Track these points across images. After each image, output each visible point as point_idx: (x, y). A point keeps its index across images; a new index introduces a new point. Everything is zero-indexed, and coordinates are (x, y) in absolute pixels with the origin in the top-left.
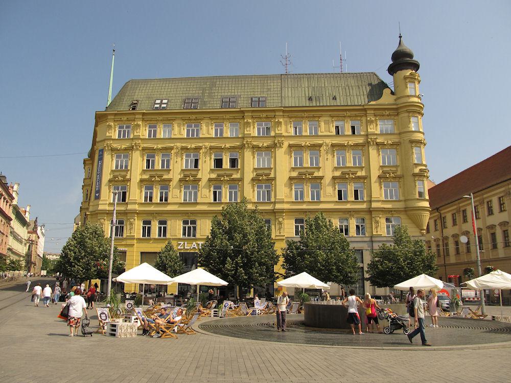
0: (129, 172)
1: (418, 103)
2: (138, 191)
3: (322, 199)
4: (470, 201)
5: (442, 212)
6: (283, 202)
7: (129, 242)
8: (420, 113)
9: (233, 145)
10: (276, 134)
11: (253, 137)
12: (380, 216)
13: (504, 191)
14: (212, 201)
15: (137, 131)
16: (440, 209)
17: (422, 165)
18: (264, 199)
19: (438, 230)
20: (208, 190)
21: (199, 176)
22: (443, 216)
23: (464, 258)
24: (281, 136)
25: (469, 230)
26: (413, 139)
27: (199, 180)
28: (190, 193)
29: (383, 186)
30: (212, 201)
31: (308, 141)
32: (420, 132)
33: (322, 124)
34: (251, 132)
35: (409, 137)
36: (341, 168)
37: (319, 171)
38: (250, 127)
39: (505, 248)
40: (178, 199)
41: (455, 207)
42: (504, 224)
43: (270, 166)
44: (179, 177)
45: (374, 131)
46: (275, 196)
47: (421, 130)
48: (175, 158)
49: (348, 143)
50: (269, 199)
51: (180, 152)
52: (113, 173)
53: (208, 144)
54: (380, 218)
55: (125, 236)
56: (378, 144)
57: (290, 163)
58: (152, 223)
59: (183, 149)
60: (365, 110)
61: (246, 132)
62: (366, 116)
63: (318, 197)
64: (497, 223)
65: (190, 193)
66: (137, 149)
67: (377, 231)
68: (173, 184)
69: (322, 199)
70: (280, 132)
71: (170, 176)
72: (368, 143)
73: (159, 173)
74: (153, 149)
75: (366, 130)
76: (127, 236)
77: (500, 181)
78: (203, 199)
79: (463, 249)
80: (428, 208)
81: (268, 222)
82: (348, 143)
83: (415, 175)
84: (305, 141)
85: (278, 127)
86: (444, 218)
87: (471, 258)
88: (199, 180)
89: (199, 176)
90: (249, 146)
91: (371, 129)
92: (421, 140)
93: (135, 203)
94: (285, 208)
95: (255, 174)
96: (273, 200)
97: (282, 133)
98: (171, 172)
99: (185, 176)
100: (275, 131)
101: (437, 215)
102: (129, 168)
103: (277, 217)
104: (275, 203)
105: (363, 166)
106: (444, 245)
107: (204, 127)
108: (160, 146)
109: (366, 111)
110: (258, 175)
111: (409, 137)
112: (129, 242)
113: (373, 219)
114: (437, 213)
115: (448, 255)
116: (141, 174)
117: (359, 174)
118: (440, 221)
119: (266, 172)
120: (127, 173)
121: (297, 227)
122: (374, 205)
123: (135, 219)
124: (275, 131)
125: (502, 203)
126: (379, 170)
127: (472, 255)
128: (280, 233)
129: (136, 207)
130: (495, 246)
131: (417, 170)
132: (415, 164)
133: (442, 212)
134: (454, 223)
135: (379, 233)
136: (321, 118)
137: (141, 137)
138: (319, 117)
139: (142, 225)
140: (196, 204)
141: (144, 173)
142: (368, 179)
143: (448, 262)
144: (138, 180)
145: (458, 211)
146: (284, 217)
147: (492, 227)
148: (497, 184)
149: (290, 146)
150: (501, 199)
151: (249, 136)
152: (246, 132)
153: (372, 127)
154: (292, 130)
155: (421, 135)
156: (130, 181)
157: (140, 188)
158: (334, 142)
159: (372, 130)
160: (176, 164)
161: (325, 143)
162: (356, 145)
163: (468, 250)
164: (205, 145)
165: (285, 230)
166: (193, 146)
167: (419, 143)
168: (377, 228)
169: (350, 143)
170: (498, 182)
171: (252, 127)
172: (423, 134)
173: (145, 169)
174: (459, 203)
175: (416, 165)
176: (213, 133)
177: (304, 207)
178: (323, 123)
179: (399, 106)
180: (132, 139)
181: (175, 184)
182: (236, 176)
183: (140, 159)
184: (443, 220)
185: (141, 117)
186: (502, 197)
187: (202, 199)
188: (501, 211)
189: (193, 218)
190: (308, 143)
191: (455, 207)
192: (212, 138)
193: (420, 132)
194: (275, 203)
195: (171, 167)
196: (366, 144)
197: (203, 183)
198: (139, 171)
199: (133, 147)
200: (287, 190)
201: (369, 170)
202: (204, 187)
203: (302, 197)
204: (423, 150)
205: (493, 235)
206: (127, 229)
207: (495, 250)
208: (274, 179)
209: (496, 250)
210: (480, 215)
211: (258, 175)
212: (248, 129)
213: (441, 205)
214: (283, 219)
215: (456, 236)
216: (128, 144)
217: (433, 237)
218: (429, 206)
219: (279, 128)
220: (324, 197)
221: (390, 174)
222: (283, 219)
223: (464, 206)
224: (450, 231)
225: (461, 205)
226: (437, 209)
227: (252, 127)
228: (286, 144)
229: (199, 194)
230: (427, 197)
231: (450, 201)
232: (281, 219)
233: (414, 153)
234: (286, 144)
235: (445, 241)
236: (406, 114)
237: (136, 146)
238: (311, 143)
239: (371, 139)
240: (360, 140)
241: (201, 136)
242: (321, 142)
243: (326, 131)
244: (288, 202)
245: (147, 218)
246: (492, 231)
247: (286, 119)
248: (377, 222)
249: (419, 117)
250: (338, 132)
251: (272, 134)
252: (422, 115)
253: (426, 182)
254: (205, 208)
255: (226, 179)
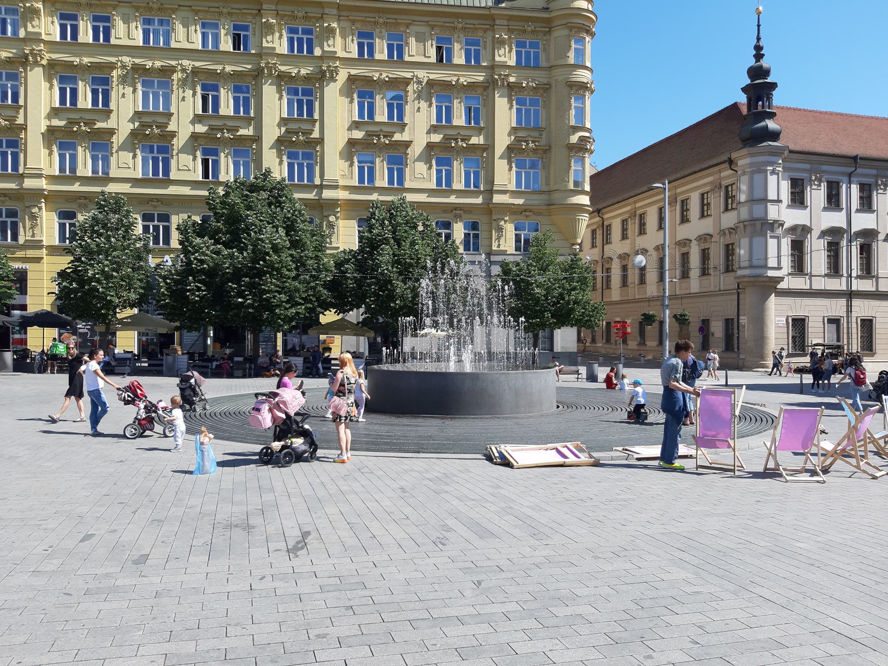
0: (22, 111)
1: (588, 11)
2: (44, 152)
3: (173, 175)
4: (662, 196)
5: (605, 216)
6: (336, 187)
7: (31, 253)
8: (589, 32)
9: (395, 76)
10: (323, 51)
11: (279, 55)
12: (507, 218)
13: (711, 182)
14: (200, 179)
15: (34, 23)
16: (604, 211)
17: (583, 129)
18: (301, 178)
19: (596, 247)
20: (191, 157)
21: (171, 127)
22: (606, 223)
23: (634, 292)
24: (332, 56)
25: (646, 247)
26: (574, 80)
27: (173, 134)
28: (301, 166)
29: (514, 165)
30: (200, 179)
31: (384, 71)
32: (586, 68)
33: (412, 41)
34: (276, 45)
35: (567, 76)
36: (210, 117)
37: (403, 130)
38: (273, 34)
39: (681, 281)
40: (132, 171)
41: (629, 208)
42: (705, 238)
43: (169, 109)
44: (131, 126)
45: (506, 59)
46: (25, 164)
47: (588, 64)
48: (181, 91)
49: (458, 80)
50: (311, 177)
51: (130, 76)
52: (140, 118)
53: (422, 74)
54: (506, 222)
55: (21, 240)
56: (511, 86)
57: (351, 112)
58: (455, 226)
59: (136, 68)
60: (492, 18)
61: (265, 44)
62: (494, 31)
63: (401, 181)
64: (693, 237)
65: (301, 166)
66: (36, 63)
67: (499, 245)
68: (117, 140)
69: (113, 173)
70: (332, 49)
71: (111, 124)
72: (495, 82)
73: (88, 116)
74: (70, 65)
75: (491, 59)
76: (26, 241)
77: (707, 165)
78: (120, 170)
79: (633, 277)
80: (587, 206)
81: (12, 214)
82: (458, 80)
83: (571, 147)
84: (455, 75)
85: (328, 39)
86: (609, 226)
87: (645, 293)
88: (173, 134)
89: (171, 127)
90: (271, 74)
91: (500, 56)
92: (588, 83)
93: (39, 176)
94: (340, 198)
95: (283, 129)
96: (317, 181)
97: (274, 48)
98: (113, 116)
99: (144, 126)
100: (322, 48)
101: (597, 222)
102: (21, 102)
103: (494, 217)
104: (321, 187)
105: (252, 116)
106: (604, 269)
107: (180, 29)
108: (86, 60)
109: (494, 20)
110: (289, 133)
111: (567, 76)
112: (31, 253)
113: (494, 224)
114: (598, 219)
115: (609, 287)
116: (49, 117)
117: (474, 140)
118: (601, 232)
119: (161, 120)
120: (18, 113)
121: (62, 227)
122: (497, 199)
123: (40, 209)
124: (322, 48)
125: (705, 202)
126: (509, 135)
127: (613, 292)
128: (33, 235)
129: (43, 184)
130: (685, 275)
131: (574, 139)
132: (573, 127)
133: (605, 216)
134: (624, 237)
135: (502, 248)
136: (411, 27)
137: (44, 37)
138: (408, 26)
139: (357, 227)
140: (169, 182)
141: (56, 114)
142: (490, 151)
143: (609, 300)
144: (43, 129)
145: (633, 215)
146: (339, 215)
147: (686, 243)
148: (702, 170)
149: (351, 79)
150: (705, 197)
151: (271, 52)
152: (265, 44)
153: (502, 51)
154: (138, 34)
155: (587, 73)
156: (26, 129)
157: (48, 146)
158: (432, 77)
159: (502, 59)
160: (122, 100)
161: (417, 77)
162: (472, 86)
163: (642, 281)
164: (121, 61)
165: (341, 237)
166: (158, 64)
167: (583, 87)
168: (499, 238)
169: (462, 80)
170: (703, 167)
171: (277, 35)
172: (591, 70)
173: (201, 113)
174: (635, 202)
175: (575, 129)
176: (197, 40)
177: (453, 199)
178: (414, 39)
179: (554, 14)
180: (24, 40)
181: (181, 143)
182: (247, 132)
183: (45, 85)
184: (607, 230)
185: (335, 11)
186: (707, 193)
187: (178, 172)
188: (702, 216)
189: (163, 210)
190: (384, 75)
191: (629, 208)
192: (197, 51)
193: (586, 68)
194: (321, 187)
195: (113, 105)
196: (489, 86)
197: (179, 142)
198: (45, 110)
199: (26, 57)
200: (344, 165)
201: (259, 128)
202: (419, 159)
203: (371, 179)
204: (588, 103)
205: (685, 257)
206: (24, 227)
207: (684, 280)
208: (321, 141)
209: (687, 280)
210: (630, 233)
211: (289, 133)
212: (269, 38)
213: (605, 204)
214: (337, 218)
215: (624, 257)
216: (14, 51)
217: (588, 258)
218: (589, 203)
219: (331, 42)
220: (410, 180)
221: (528, 144)
222: (337, 218)
223: (642, 207)
224: (617, 247)
225: (638, 205)
226: (599, 211)
227: (277, 35)
228: (342, 76)
229: (173, 163)
230: (587, 188)
231: (620, 198)
232: (332, 218)
233: (573, 107)
234: (342, 76)
235: (606, 266)
236: (565, 32)
237: (34, 56)
238: (391, 76)
239: (500, 75)
240: (480, 77)
241: (173, 45)
242: (408, 75)
243: (418, 54)
244: (346, 188)
245: (68, 208)
246: (684, 250)
247: (344, 24)
248: (500, 229)
249: (587, 39)
250: (440, 59)
251: (317, 52)
252: (592, 35)
253: (587, 161)
254: (186, 191)
255: (226, 135)
